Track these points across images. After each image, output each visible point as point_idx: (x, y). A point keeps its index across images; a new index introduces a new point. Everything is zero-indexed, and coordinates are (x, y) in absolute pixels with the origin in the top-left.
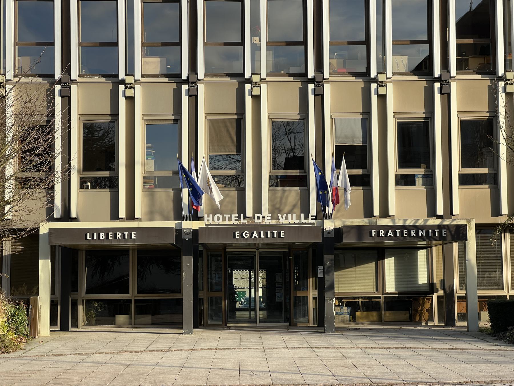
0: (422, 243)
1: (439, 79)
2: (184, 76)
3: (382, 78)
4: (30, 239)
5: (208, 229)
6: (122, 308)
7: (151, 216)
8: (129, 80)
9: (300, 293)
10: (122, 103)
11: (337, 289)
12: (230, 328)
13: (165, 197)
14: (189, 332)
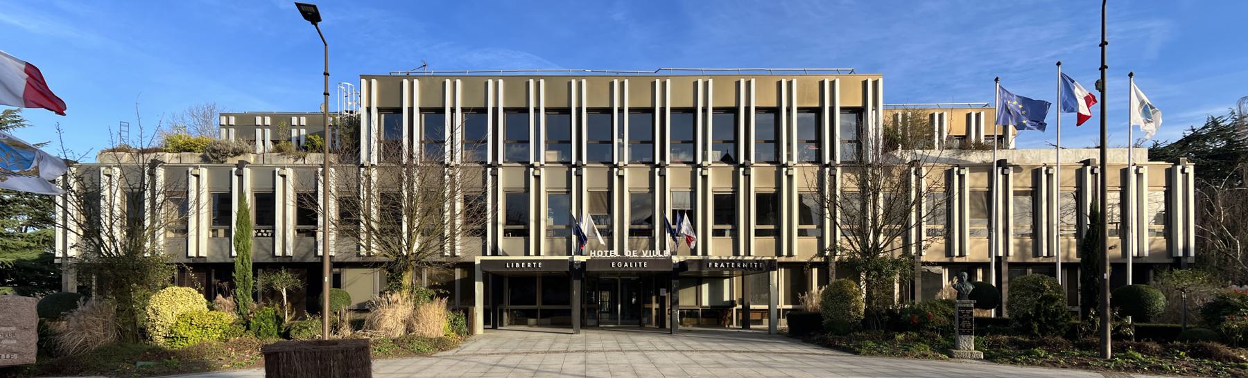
0: (726, 273)
1: (743, 166)
2: (574, 162)
3: (705, 164)
4: (468, 267)
5: (593, 261)
6: (532, 314)
7: (552, 253)
8: (537, 164)
9: (647, 306)
10: (532, 179)
11: (681, 303)
12: (602, 329)
13: (560, 242)
14: (578, 332)
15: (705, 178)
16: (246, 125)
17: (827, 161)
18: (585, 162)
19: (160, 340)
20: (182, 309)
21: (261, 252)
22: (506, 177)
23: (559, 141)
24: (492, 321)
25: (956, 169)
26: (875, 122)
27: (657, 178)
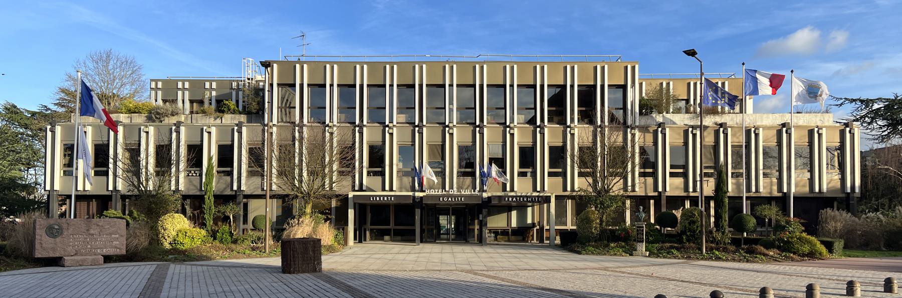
1: (539, 127)
3: (512, 125)
4: (344, 200)
6: (387, 232)
8: (391, 125)
9: (471, 227)
10: (387, 135)
13: (407, 180)
15: (512, 135)
16: (169, 89)
17: (599, 123)
18: (425, 123)
19: (167, 245)
20: (179, 227)
21: (192, 187)
22: (369, 135)
23: (406, 107)
24: (360, 238)
25: (690, 129)
26: (633, 97)
27: (478, 135)
